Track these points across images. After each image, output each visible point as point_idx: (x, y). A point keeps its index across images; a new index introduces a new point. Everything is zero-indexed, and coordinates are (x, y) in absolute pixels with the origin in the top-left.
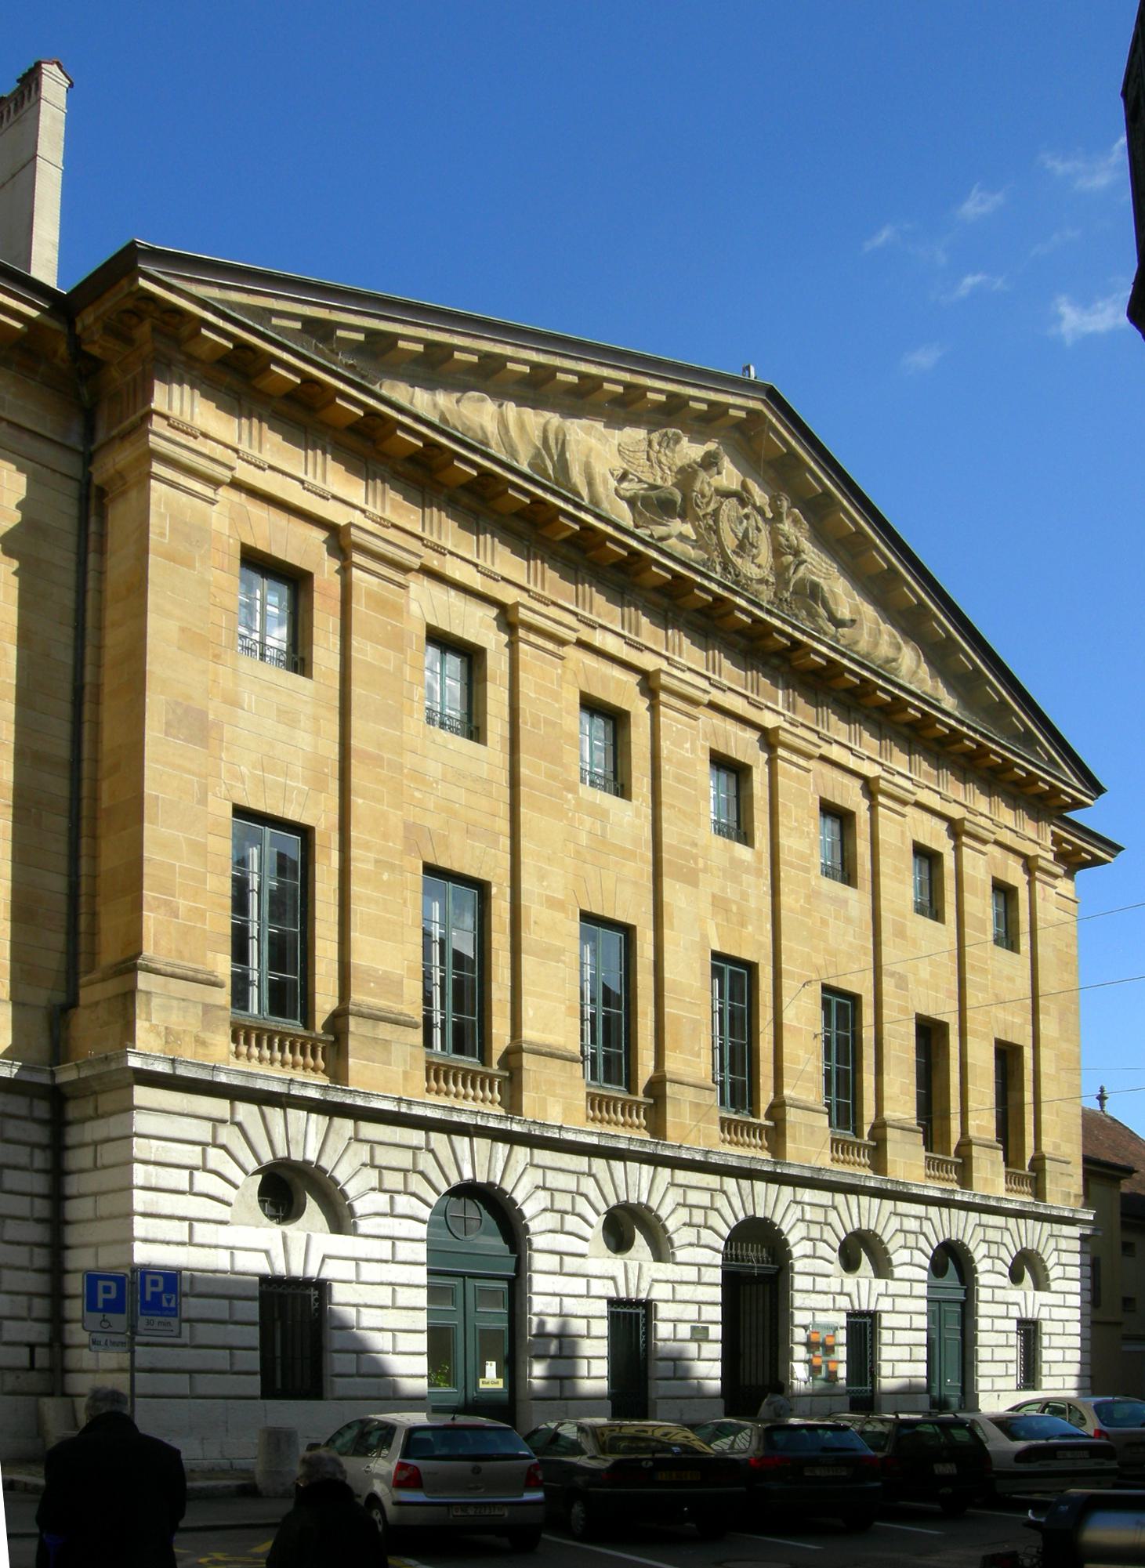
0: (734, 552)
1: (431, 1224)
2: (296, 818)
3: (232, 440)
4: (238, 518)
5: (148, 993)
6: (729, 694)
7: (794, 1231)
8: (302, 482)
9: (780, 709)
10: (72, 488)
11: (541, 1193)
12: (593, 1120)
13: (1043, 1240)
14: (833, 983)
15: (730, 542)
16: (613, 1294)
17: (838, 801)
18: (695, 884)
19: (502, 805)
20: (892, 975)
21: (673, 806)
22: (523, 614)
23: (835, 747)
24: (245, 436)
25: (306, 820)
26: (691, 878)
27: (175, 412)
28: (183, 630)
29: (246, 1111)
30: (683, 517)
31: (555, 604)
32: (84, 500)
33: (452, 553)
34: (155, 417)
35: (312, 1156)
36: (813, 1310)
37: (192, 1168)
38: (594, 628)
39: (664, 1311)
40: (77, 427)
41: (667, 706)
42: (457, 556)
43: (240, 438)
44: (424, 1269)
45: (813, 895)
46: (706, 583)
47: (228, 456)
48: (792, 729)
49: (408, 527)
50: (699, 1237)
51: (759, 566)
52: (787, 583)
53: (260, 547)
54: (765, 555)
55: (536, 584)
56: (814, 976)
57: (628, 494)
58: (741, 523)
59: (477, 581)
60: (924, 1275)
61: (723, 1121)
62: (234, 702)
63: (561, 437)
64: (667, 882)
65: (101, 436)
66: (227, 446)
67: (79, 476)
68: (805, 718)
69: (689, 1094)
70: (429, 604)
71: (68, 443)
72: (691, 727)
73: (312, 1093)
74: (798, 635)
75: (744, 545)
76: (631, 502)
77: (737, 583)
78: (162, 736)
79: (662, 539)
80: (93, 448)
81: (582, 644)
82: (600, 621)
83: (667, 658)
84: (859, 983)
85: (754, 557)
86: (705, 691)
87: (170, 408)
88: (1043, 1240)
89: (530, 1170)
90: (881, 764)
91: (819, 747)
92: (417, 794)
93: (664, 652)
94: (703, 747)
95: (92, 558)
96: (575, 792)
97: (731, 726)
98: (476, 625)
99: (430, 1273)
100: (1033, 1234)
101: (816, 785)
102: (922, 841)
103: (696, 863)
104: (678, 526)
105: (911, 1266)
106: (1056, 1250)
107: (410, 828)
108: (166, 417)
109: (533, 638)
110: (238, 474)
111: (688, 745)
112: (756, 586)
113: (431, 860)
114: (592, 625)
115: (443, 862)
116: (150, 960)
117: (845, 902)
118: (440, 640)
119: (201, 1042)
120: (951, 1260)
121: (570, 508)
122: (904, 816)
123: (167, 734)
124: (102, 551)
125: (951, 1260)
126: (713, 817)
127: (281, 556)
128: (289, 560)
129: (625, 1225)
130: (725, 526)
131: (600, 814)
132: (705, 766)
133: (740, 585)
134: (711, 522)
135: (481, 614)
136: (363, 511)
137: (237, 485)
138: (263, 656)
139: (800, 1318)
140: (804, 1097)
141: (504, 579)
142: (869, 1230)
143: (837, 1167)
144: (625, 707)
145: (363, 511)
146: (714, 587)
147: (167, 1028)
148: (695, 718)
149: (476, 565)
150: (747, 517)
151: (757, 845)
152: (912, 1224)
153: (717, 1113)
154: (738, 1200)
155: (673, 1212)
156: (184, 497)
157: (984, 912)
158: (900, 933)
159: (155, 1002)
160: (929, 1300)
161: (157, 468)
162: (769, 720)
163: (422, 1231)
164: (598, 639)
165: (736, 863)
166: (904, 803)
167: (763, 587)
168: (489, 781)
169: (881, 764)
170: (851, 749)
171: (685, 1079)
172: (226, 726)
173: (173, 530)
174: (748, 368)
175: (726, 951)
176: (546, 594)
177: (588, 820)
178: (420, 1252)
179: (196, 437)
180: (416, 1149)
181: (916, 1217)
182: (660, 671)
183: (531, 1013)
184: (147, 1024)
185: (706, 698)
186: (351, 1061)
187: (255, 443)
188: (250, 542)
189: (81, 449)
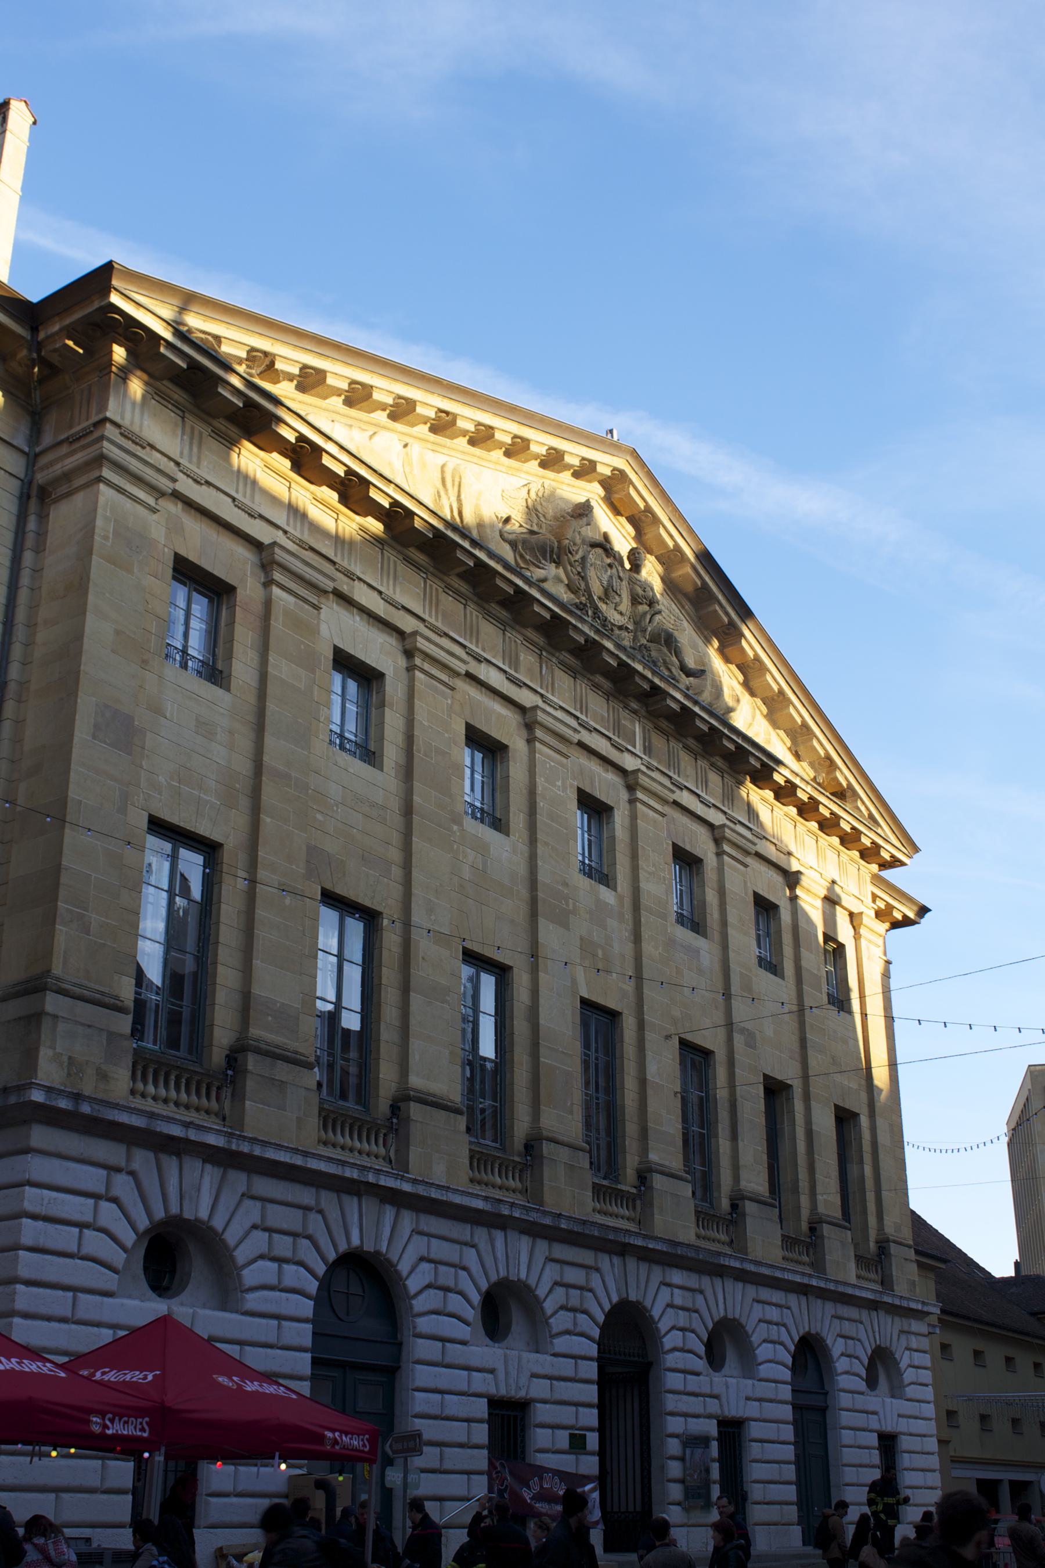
0: (600, 598)
1: (317, 1300)
2: (207, 834)
3: (175, 453)
4: (174, 528)
5: (55, 1017)
6: (595, 735)
7: (664, 1319)
8: (234, 499)
9: (638, 753)
10: (14, 485)
11: (425, 1266)
12: (325, 1143)
13: (895, 1337)
14: (689, 1037)
15: (597, 590)
16: (493, 1391)
17: (688, 848)
18: (566, 926)
19: (395, 833)
20: (742, 1031)
21: (546, 844)
22: (421, 643)
23: (685, 793)
24: (186, 451)
25: (216, 836)
26: (563, 920)
27: (126, 422)
28: (118, 632)
29: (142, 1160)
30: (558, 563)
31: (446, 635)
32: (24, 498)
33: (360, 579)
34: (108, 425)
35: (203, 1214)
36: (686, 1415)
37: (82, 1226)
38: (480, 661)
39: (542, 1413)
40: (24, 429)
41: (542, 742)
42: (365, 582)
43: (182, 453)
44: (308, 1356)
45: (671, 943)
46: (579, 625)
47: (170, 467)
48: (649, 773)
49: (324, 551)
50: (575, 1324)
51: (621, 614)
52: (644, 631)
53: (191, 558)
54: (625, 605)
55: (430, 616)
56: (673, 1031)
57: (511, 537)
58: (606, 571)
59: (378, 607)
60: (786, 1375)
61: (595, 1185)
62: (158, 710)
63: (457, 480)
64: (542, 922)
65: (47, 440)
66: (170, 459)
67: (22, 476)
68: (659, 762)
69: (564, 1154)
70: (338, 627)
71: (15, 443)
72: (563, 766)
73: (212, 1139)
74: (657, 681)
75: (609, 592)
76: (513, 544)
77: (604, 626)
78: (90, 739)
79: (544, 580)
80: (38, 450)
81: (470, 676)
82: (485, 655)
83: (542, 696)
84: (711, 1039)
85: (617, 605)
86: (575, 730)
87: (123, 418)
88: (895, 1337)
89: (416, 1237)
90: (725, 813)
91: (673, 792)
92: (319, 817)
93: (539, 690)
94: (571, 786)
95: (28, 557)
96: (460, 823)
97: (594, 766)
98: (377, 650)
99: (315, 1362)
100: (887, 1329)
101: (668, 831)
102: (761, 893)
103: (567, 905)
104: (551, 570)
105: (775, 1360)
106: (907, 1349)
107: (312, 851)
108: (117, 425)
109: (426, 666)
110: (179, 487)
111: (559, 783)
112: (617, 632)
113: (328, 886)
114: (479, 659)
115: (340, 890)
116: (58, 979)
117: (697, 951)
118: (344, 662)
119: (103, 1076)
120: (809, 1354)
121: (466, 545)
122: (746, 866)
123: (94, 737)
124: (39, 549)
125: (809, 1354)
126: (580, 858)
127: (209, 568)
128: (216, 573)
129: (501, 1309)
130: (591, 573)
131: (482, 849)
132: (574, 804)
133: (605, 626)
134: (579, 569)
135: (381, 640)
136: (285, 532)
137: (177, 495)
138: (184, 666)
139: (675, 1425)
140: (667, 1163)
141: (403, 607)
142: (734, 1319)
143: (703, 1244)
144: (505, 742)
145: (285, 532)
146: (586, 629)
147: (70, 1058)
148: (567, 757)
149: (380, 593)
150: (610, 566)
151: (619, 889)
152: (773, 1314)
153: (589, 1178)
154: (608, 1283)
155: (550, 1291)
156: (129, 504)
157: (819, 970)
158: (747, 987)
159: (61, 1026)
160: (796, 1407)
161: (107, 473)
162: (630, 763)
163: (307, 1307)
164: (484, 672)
165: (600, 904)
166: (747, 853)
167: (624, 634)
168: (384, 808)
169: (725, 813)
170: (698, 796)
171: (561, 1138)
172: (148, 734)
173: (116, 533)
174: (611, 431)
175: (594, 998)
176: (439, 625)
177: (471, 855)
178: (304, 1334)
179: (143, 448)
180: (307, 1209)
181: (776, 1305)
182: (537, 707)
183: (417, 1057)
184: (50, 1053)
185: (576, 738)
186: (248, 1103)
187: (195, 459)
188: (183, 552)
189: (26, 449)
